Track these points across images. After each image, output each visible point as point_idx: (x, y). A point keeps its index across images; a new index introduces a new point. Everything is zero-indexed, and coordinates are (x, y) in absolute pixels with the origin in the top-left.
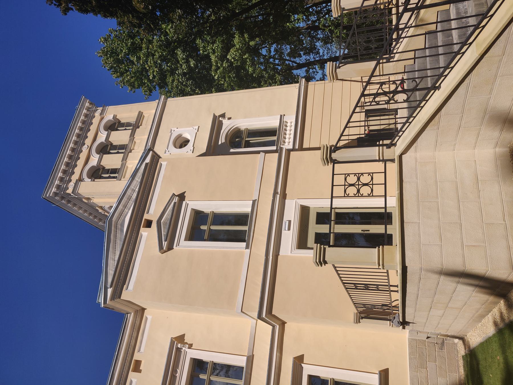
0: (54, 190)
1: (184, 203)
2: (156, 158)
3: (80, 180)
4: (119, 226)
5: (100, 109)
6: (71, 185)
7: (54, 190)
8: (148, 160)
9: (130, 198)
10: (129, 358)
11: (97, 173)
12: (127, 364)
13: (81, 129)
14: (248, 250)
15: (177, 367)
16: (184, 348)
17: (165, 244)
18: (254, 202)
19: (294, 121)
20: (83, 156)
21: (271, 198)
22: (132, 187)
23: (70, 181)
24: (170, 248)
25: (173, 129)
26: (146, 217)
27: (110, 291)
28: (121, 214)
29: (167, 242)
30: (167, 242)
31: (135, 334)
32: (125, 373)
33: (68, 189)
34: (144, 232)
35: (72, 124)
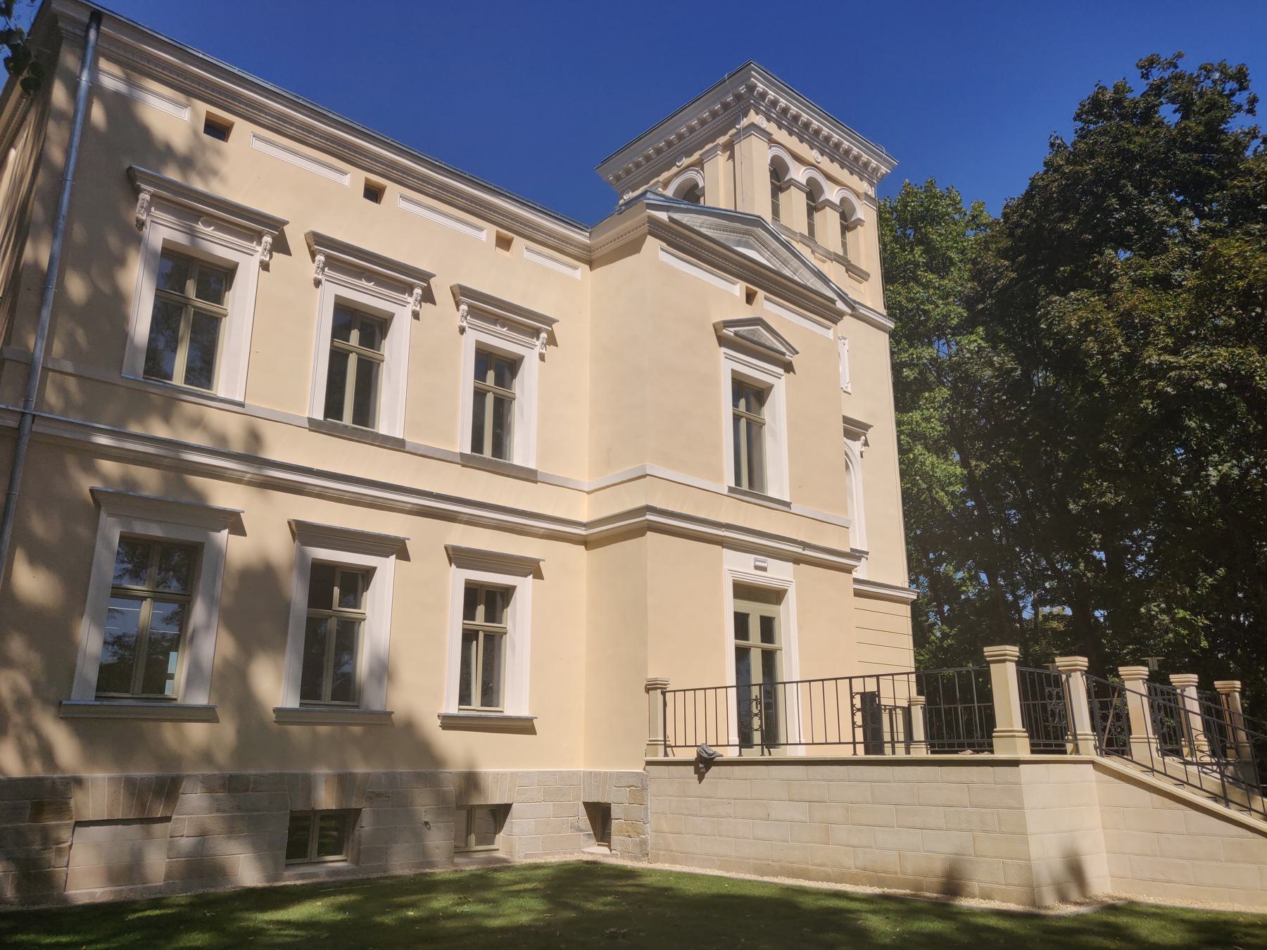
0: (761, 87)
1: (781, 371)
2: (835, 317)
3: (772, 142)
5: (871, 192)
7: (761, 87)
8: (840, 305)
9: (785, 263)
10: (516, 226)
11: (778, 172)
12: (507, 222)
14: (726, 492)
15: (220, 228)
16: (260, 249)
17: (729, 332)
18: (787, 504)
20: (813, 155)
21: (799, 539)
22: (803, 270)
24: (723, 341)
26: (761, 294)
27: (663, 216)
28: (764, 244)
29: (736, 338)
30: (736, 338)
31: (551, 242)
33: (757, 114)
34: (738, 289)
35: (858, 136)
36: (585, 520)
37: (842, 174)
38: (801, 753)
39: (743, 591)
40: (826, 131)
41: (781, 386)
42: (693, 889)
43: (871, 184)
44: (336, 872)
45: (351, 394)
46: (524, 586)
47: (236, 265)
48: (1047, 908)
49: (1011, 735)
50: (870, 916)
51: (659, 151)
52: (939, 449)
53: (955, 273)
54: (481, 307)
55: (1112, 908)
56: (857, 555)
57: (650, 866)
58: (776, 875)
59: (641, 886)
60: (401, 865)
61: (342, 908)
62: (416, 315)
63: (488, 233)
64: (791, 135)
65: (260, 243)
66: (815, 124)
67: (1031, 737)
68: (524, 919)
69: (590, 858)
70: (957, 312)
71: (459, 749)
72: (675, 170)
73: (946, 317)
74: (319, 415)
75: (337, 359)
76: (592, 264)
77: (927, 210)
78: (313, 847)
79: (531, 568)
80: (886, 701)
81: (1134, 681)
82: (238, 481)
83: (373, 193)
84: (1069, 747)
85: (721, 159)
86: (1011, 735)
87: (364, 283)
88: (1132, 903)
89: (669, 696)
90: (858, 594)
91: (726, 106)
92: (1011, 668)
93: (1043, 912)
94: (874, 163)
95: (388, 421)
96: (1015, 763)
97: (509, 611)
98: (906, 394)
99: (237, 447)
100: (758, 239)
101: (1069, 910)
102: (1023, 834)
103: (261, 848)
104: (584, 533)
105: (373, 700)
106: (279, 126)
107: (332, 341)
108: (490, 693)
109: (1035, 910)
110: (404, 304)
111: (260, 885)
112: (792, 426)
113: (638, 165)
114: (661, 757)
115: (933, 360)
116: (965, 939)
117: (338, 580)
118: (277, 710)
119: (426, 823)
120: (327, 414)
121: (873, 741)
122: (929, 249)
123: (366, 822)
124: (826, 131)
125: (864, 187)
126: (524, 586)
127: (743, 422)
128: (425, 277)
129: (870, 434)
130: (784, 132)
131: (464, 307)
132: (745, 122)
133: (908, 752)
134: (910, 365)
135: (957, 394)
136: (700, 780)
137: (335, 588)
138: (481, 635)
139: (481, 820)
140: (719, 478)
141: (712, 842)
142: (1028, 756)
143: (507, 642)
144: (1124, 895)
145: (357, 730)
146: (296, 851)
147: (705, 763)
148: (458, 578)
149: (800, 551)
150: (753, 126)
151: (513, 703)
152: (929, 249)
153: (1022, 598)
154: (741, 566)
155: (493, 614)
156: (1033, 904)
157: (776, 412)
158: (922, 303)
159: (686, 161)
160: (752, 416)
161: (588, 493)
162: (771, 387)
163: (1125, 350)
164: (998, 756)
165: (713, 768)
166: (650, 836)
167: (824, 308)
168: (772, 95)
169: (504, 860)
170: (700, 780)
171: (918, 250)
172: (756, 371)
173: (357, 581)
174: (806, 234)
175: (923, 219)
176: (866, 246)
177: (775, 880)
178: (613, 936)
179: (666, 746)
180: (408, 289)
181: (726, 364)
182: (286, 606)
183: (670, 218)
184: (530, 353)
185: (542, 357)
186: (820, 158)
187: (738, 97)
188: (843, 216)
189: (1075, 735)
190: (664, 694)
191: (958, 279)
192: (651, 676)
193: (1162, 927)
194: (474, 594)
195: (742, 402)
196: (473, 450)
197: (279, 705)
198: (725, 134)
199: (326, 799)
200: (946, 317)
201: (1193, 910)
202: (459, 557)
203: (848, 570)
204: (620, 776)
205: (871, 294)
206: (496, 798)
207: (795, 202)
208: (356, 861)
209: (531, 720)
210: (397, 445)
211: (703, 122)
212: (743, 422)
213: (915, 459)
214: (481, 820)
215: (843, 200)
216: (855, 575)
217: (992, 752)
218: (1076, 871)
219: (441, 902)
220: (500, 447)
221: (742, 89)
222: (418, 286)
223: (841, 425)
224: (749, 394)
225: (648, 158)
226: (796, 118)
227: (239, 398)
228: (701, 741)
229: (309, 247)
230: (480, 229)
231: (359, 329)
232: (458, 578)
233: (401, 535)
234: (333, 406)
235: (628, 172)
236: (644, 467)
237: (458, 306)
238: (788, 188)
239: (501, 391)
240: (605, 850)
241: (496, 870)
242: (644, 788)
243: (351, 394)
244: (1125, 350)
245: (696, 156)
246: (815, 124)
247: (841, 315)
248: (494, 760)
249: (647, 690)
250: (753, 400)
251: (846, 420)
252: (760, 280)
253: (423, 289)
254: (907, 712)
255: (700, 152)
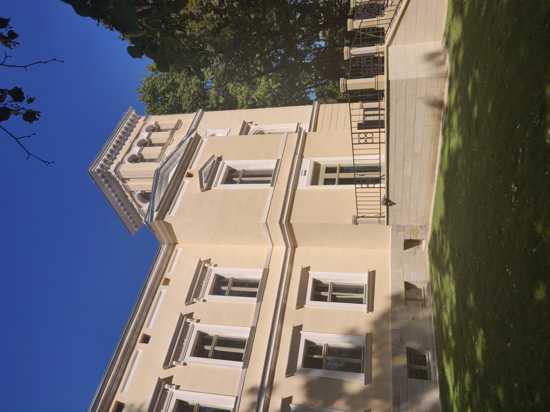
0: (98, 167)
1: (221, 162)
3: (122, 162)
4: (164, 177)
5: (143, 118)
6: (113, 167)
7: (98, 167)
8: (193, 136)
9: (175, 160)
10: (160, 276)
11: (135, 159)
12: (158, 280)
13: (115, 147)
14: (273, 188)
16: (170, 390)
17: (205, 185)
18: (278, 160)
19: (308, 126)
21: (293, 156)
22: (178, 152)
23: (112, 163)
24: (209, 188)
25: (208, 131)
26: (188, 170)
27: (155, 214)
29: (207, 183)
30: (207, 183)
31: (166, 261)
32: (155, 287)
33: (110, 168)
34: (186, 181)
36: (285, 248)
37: (136, 130)
38: (384, 157)
39: (315, 181)
40: (117, 138)
41: (228, 162)
42: (441, 211)
43: (140, 118)
44: (433, 358)
45: (232, 350)
46: (313, 275)
47: (177, 400)
48: (447, 71)
49: (377, 83)
50: (451, 145)
51: (125, 209)
52: (253, 86)
53: (177, 80)
54: (194, 293)
55: (447, 44)
56: (299, 130)
57: (431, 224)
58: (434, 175)
59: (439, 232)
60: (431, 328)
61: (448, 360)
62: (198, 321)
63: (163, 289)
64: (119, 154)
65: (168, 390)
66: (114, 143)
67: (377, 75)
68: (453, 288)
69: (427, 248)
70: (195, 80)
71: (382, 303)
72: (133, 203)
73: (197, 84)
74: (241, 364)
75: (218, 355)
76: (175, 243)
77: (150, 92)
78: (423, 368)
79: (305, 271)
80: (361, 119)
81: (354, 24)
82: (269, 399)
83: (146, 339)
84: (381, 55)
85: (129, 183)
86: (377, 83)
87: (185, 344)
88: (445, 34)
89: (359, 215)
90: (315, 130)
91: (106, 182)
92: (349, 82)
93: (449, 74)
94: (131, 117)
95: (243, 334)
96: (388, 82)
97: (324, 281)
98: (231, 104)
99: (255, 398)
100: (165, 171)
101: (448, 62)
102: (417, 80)
103: (425, 390)
104: (290, 248)
105: (361, 342)
106: (117, 381)
107: (209, 358)
108: (358, 290)
109: (448, 77)
110: (193, 326)
111: (438, 389)
112: (244, 158)
113: (131, 218)
114: (385, 219)
115: (216, 88)
116: (460, 110)
117: (310, 356)
118: (366, 384)
119: (413, 319)
120: (240, 360)
121: (378, 124)
122: (168, 91)
123: (414, 345)
124: (117, 138)
125: (141, 121)
126: (313, 275)
127: (243, 179)
128: (182, 317)
129: (247, 121)
130: (118, 156)
131: (195, 300)
132: (113, 174)
133: (383, 109)
134: (217, 98)
135: (231, 80)
136: (394, 204)
137: (315, 357)
138: (334, 293)
139: (411, 294)
140: (267, 191)
141: (422, 199)
142: (385, 76)
143: (337, 282)
144: (442, 37)
145: (374, 347)
146: (424, 375)
147: (388, 202)
148: (310, 304)
149: (298, 156)
150: (115, 170)
151: (362, 280)
152: (168, 91)
153: (315, 46)
154: (304, 181)
155: (325, 288)
156: (446, 77)
157: (239, 165)
158: (190, 94)
159: (130, 198)
160: (241, 175)
161: (273, 246)
162: (228, 167)
163: (212, 13)
164: (385, 88)
165: (390, 199)
166: (419, 224)
167: (193, 143)
168: (102, 162)
169: (428, 284)
170: (394, 204)
171: (167, 96)
172: (221, 173)
173: (311, 348)
174: (161, 147)
175: (154, 93)
176: (167, 121)
177: (436, 176)
178: (460, 255)
179: (380, 217)
180: (187, 324)
181: (219, 187)
182: (321, 379)
183: (156, 211)
184: (214, 271)
185: (216, 266)
186: (129, 141)
187: (103, 176)
188: (154, 130)
189: (376, 53)
190: (358, 217)
191: (179, 78)
192: (351, 222)
193: (455, 28)
194: (317, 297)
195: (235, 179)
196: (255, 297)
197: (363, 382)
198: (118, 182)
199: (403, 360)
200: (197, 84)
201: (448, 12)
202: (301, 304)
203: (306, 134)
204: (393, 236)
205: (188, 119)
206: (402, 287)
207: (148, 152)
208: (429, 350)
209: (369, 273)
210: (253, 330)
211: (113, 191)
212: (243, 179)
213: (258, 98)
214: (411, 294)
215: (147, 131)
216: (307, 131)
217: (383, 90)
218: (432, 57)
219: (446, 318)
220: (254, 284)
221: (99, 175)
222: (186, 320)
223: (243, 136)
224: (231, 176)
225: (128, 214)
226: (112, 151)
227: (234, 399)
228: (378, 203)
229: (170, 368)
230: (161, 292)
231: (204, 346)
232: (310, 304)
233: (292, 329)
234: (237, 357)
235: (134, 222)
236: (263, 224)
237: (194, 303)
238: (141, 155)
239: (230, 283)
240: (424, 242)
241: (432, 289)
242: (398, 226)
243: (232, 350)
244: (212, 13)
245: (127, 194)
246: (114, 143)
247: (197, 135)
248: (386, 290)
249: (357, 224)
250: (234, 174)
251: (241, 134)
252: (182, 171)
253: (187, 318)
254: (366, 110)
255: (126, 192)
